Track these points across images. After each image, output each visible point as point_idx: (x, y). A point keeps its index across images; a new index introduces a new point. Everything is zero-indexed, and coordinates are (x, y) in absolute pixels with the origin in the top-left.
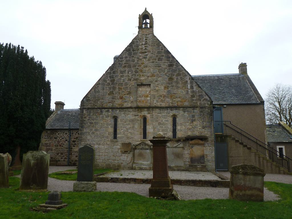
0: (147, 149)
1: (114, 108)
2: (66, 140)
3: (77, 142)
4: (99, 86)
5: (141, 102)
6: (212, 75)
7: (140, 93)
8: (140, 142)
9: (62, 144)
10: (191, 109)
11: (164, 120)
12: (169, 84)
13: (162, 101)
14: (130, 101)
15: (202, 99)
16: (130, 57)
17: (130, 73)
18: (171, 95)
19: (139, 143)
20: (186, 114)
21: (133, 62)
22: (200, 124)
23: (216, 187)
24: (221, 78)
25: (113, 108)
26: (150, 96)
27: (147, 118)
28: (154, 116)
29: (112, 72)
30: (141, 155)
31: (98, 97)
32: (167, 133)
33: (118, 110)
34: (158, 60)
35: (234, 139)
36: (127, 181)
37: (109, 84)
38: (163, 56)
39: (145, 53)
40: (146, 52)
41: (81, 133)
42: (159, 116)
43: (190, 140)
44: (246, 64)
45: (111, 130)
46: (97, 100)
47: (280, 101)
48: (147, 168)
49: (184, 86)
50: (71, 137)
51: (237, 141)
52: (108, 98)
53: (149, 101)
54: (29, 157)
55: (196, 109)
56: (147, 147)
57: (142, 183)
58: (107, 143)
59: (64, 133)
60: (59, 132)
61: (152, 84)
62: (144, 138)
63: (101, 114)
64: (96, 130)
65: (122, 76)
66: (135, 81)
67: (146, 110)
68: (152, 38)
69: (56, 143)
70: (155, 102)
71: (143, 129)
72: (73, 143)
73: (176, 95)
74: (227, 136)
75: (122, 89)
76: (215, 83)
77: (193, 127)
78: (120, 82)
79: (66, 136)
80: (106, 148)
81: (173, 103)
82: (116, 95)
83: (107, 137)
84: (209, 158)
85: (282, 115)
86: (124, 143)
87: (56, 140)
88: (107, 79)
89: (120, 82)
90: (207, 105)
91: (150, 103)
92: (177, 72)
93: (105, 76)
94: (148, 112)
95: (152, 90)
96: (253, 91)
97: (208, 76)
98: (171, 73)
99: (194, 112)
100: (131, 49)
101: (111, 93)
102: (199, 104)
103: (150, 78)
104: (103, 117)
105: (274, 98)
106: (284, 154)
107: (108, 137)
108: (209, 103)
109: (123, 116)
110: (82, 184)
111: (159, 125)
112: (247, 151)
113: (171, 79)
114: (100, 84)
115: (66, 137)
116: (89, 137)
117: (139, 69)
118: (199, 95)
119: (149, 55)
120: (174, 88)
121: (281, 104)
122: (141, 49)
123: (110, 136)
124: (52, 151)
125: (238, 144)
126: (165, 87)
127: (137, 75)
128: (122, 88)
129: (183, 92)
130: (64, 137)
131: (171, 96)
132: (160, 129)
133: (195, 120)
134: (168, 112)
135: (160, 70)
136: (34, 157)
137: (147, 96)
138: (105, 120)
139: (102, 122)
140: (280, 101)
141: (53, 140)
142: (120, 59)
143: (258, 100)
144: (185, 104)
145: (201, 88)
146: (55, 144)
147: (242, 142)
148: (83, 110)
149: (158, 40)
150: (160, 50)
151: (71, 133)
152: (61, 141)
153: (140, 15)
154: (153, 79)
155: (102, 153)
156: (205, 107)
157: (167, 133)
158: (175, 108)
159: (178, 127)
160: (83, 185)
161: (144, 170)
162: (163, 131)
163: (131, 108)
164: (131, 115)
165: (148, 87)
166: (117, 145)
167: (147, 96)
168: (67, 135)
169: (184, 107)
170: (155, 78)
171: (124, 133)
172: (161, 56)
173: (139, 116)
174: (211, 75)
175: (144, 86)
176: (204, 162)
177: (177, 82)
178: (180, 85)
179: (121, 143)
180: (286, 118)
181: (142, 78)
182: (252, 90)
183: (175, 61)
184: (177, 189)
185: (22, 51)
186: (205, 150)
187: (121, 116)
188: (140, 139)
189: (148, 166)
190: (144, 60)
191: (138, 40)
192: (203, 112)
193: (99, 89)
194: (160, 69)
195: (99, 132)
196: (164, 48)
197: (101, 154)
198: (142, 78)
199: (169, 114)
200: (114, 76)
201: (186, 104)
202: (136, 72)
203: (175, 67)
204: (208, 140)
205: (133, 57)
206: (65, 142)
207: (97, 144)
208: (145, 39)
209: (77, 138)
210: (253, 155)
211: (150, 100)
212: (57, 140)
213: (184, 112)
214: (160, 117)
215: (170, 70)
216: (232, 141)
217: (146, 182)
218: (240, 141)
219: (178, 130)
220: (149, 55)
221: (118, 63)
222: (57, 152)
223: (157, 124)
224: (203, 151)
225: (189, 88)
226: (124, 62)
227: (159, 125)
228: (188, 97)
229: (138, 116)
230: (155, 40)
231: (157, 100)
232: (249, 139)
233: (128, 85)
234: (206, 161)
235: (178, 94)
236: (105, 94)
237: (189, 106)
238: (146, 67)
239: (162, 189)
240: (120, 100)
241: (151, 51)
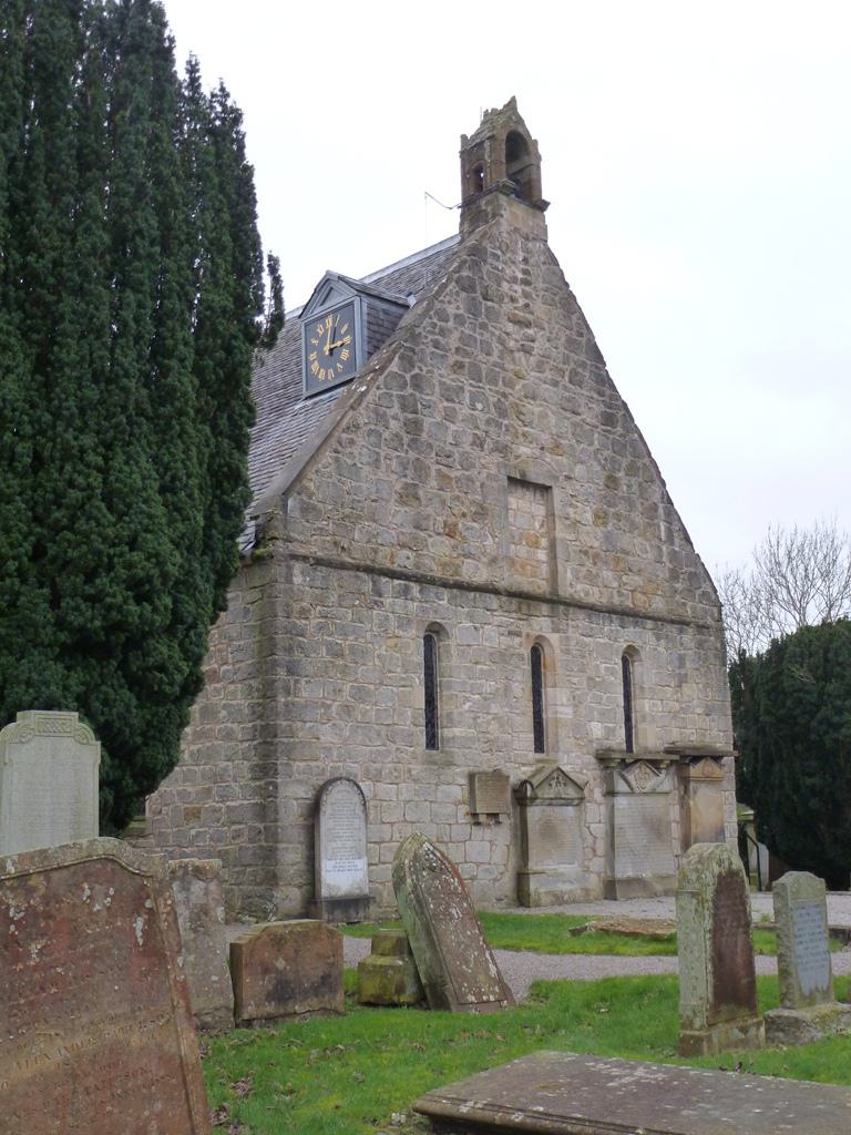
5: (518, 566)
33: (446, 593)
94: (553, 622)
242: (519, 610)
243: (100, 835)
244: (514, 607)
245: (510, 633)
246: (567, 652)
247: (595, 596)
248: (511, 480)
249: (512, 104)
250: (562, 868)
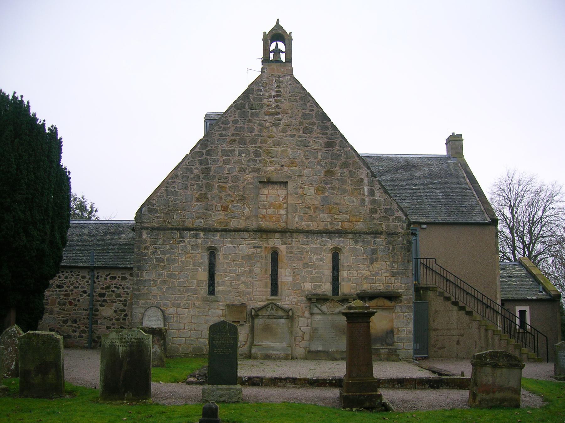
0: (281, 317)
1: (210, 230)
2: (85, 292)
3: (109, 296)
4: (175, 180)
5: (267, 218)
6: (394, 156)
7: (264, 199)
8: (265, 303)
9: (74, 300)
10: (369, 238)
11: (315, 257)
12: (327, 183)
13: (311, 219)
14: (244, 215)
15: (391, 218)
16: (244, 122)
17: (244, 155)
18: (328, 206)
19: (262, 304)
20: (359, 247)
21: (251, 132)
22: (387, 267)
23: (438, 388)
24: (413, 163)
25: (206, 230)
26: (285, 206)
27: (280, 253)
28: (295, 249)
29: (204, 152)
30: (267, 329)
31: (174, 204)
32: (321, 285)
33: (218, 235)
34: (303, 133)
35: (441, 294)
36: (279, 384)
37: (198, 176)
38: (314, 124)
39: (277, 115)
40: (279, 113)
41: (137, 280)
42: (304, 249)
43: (367, 299)
44: (461, 135)
45: (204, 276)
46: (171, 210)
47: (512, 204)
48: (281, 356)
49: (356, 189)
50: (95, 285)
51: (447, 299)
52: (196, 207)
53: (284, 217)
54: (113, 340)
55: (378, 237)
56: (281, 313)
57: (308, 385)
58: (194, 304)
59: (79, 275)
60: (67, 272)
61: (291, 183)
62: (272, 295)
63: (181, 241)
64: (171, 276)
65: (226, 162)
66: (255, 174)
67: (277, 235)
68: (290, 84)
69: (62, 297)
70: (297, 219)
71: (271, 275)
72: (100, 299)
73: (340, 206)
74: (427, 289)
75: (227, 190)
76: (401, 173)
77: (374, 273)
78: (223, 173)
79: (83, 282)
80: (192, 313)
81: (334, 224)
82: (214, 202)
83: (195, 292)
84: (403, 335)
85: (515, 235)
86: (233, 305)
87: (60, 291)
89: (223, 173)
90: (400, 230)
91: (286, 222)
93: (188, 159)
94: (282, 241)
95: (291, 194)
96: (476, 195)
97: (385, 156)
98: (330, 160)
99: (375, 244)
100: (247, 103)
101: (202, 198)
102: (384, 227)
103: (286, 169)
104: (185, 249)
105: (502, 198)
106: (528, 321)
107: (197, 290)
108: (405, 225)
109: (229, 247)
110: (218, 389)
111: (304, 267)
112: (466, 318)
113: (329, 173)
114: (177, 176)
115: (82, 285)
116: (154, 290)
117: (264, 148)
118: (386, 210)
119: (285, 120)
120: (335, 192)
121: (514, 212)
122: (268, 106)
123: (201, 289)
124: (52, 314)
125: (449, 304)
126: (317, 190)
127: (258, 162)
128: (226, 188)
129: (353, 202)
130: (80, 284)
131: (330, 210)
132: (307, 277)
133: (376, 260)
134: (322, 241)
135: (307, 153)
136: (124, 340)
137: (280, 207)
138: (189, 255)
139: (183, 259)
140: (512, 204)
141: (53, 291)
142: (221, 125)
143: (486, 215)
144: (357, 227)
145: (389, 195)
146: (59, 300)
147: (457, 300)
148: (141, 232)
149: (304, 90)
150: (308, 111)
151: (96, 277)
152: (72, 294)
153: (265, 33)
154: (292, 171)
155: (185, 323)
156: (396, 234)
157: (321, 285)
158: (337, 233)
159: (344, 274)
160: (222, 392)
161: (274, 359)
162: (312, 280)
163: (245, 230)
164: (245, 246)
165: (282, 186)
166: (216, 307)
167: (280, 207)
168: (85, 280)
169: (357, 233)
170: (296, 168)
171: (230, 283)
172: (310, 124)
173: (263, 249)
174: (391, 156)
175: (273, 185)
176: (393, 343)
177: (342, 181)
178: (348, 187)
179: (225, 303)
180: (523, 242)
181: (270, 169)
182: (475, 193)
183: (339, 135)
184: (388, 395)
185: (22, 101)
186: (395, 319)
187: (227, 247)
188: (264, 297)
189: (282, 352)
190: (274, 129)
191: (262, 86)
192: (392, 245)
193: (176, 186)
195: (178, 279)
196: (315, 108)
197: (182, 326)
198: (270, 169)
199: (325, 245)
200: (209, 161)
201: (360, 226)
202: (257, 154)
203: (339, 148)
204: (401, 300)
205: (250, 121)
206: (81, 296)
207: (173, 305)
208: (276, 85)
209: (108, 287)
210: (475, 325)
211: (287, 215)
212: (63, 291)
213: (356, 242)
214: (307, 252)
215: (328, 153)
216: (438, 298)
217: (315, 384)
218: (453, 299)
219: (343, 279)
220: (285, 120)
221: (218, 133)
222: (62, 317)
223: (301, 266)
224: (392, 321)
225: (366, 193)
226: (230, 133)
227: (304, 267)
228: (365, 211)
229: (260, 247)
230: (296, 90)
231: (302, 217)
232: (468, 293)
233: (240, 182)
234: (396, 340)
235: (343, 205)
236: (189, 199)
237: (365, 230)
238: (278, 145)
239: (365, 395)
240: (222, 213)
241: (289, 112)
242: (261, 237)
248: (260, 182)
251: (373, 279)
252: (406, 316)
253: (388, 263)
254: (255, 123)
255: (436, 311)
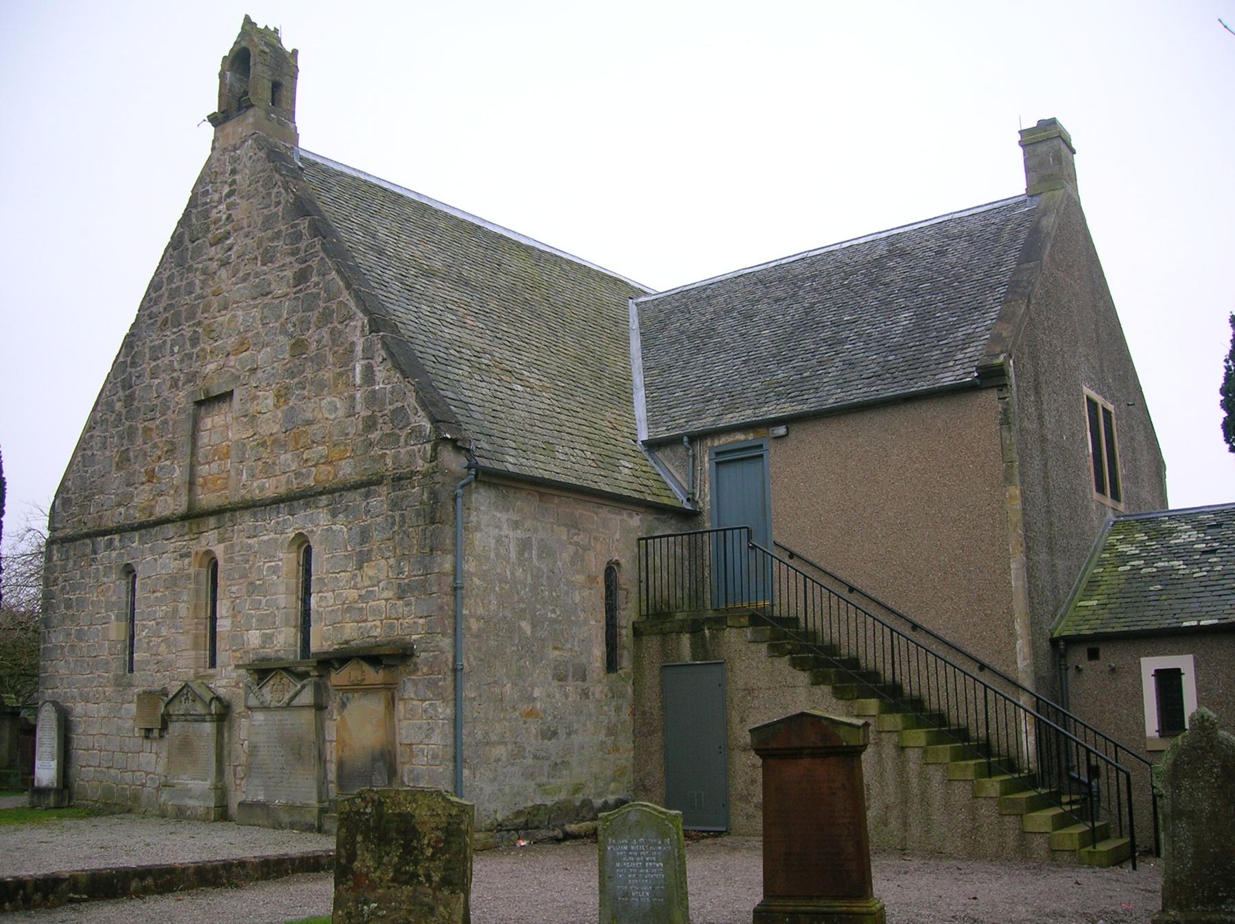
0: (201, 719)
33: (137, 535)
39: (227, 238)
75: (154, 435)
77: (363, 592)
88: (115, 398)
92: (322, 305)
102: (389, 461)
111: (250, 594)
113: (299, 346)
157: (273, 634)
189: (201, 803)
194: (265, 306)
204: (415, 664)
208: (229, 168)
216: (753, 647)
225: (358, 381)
241: (245, 223)
243: (750, 731)
244: (186, 530)
245: (182, 556)
246: (231, 560)
247: (270, 487)
248: (199, 403)
249: (247, 20)
250: (192, 784)
251: (361, 609)
252: (425, 711)
253: (392, 561)
254: (197, 269)
255: (749, 691)
